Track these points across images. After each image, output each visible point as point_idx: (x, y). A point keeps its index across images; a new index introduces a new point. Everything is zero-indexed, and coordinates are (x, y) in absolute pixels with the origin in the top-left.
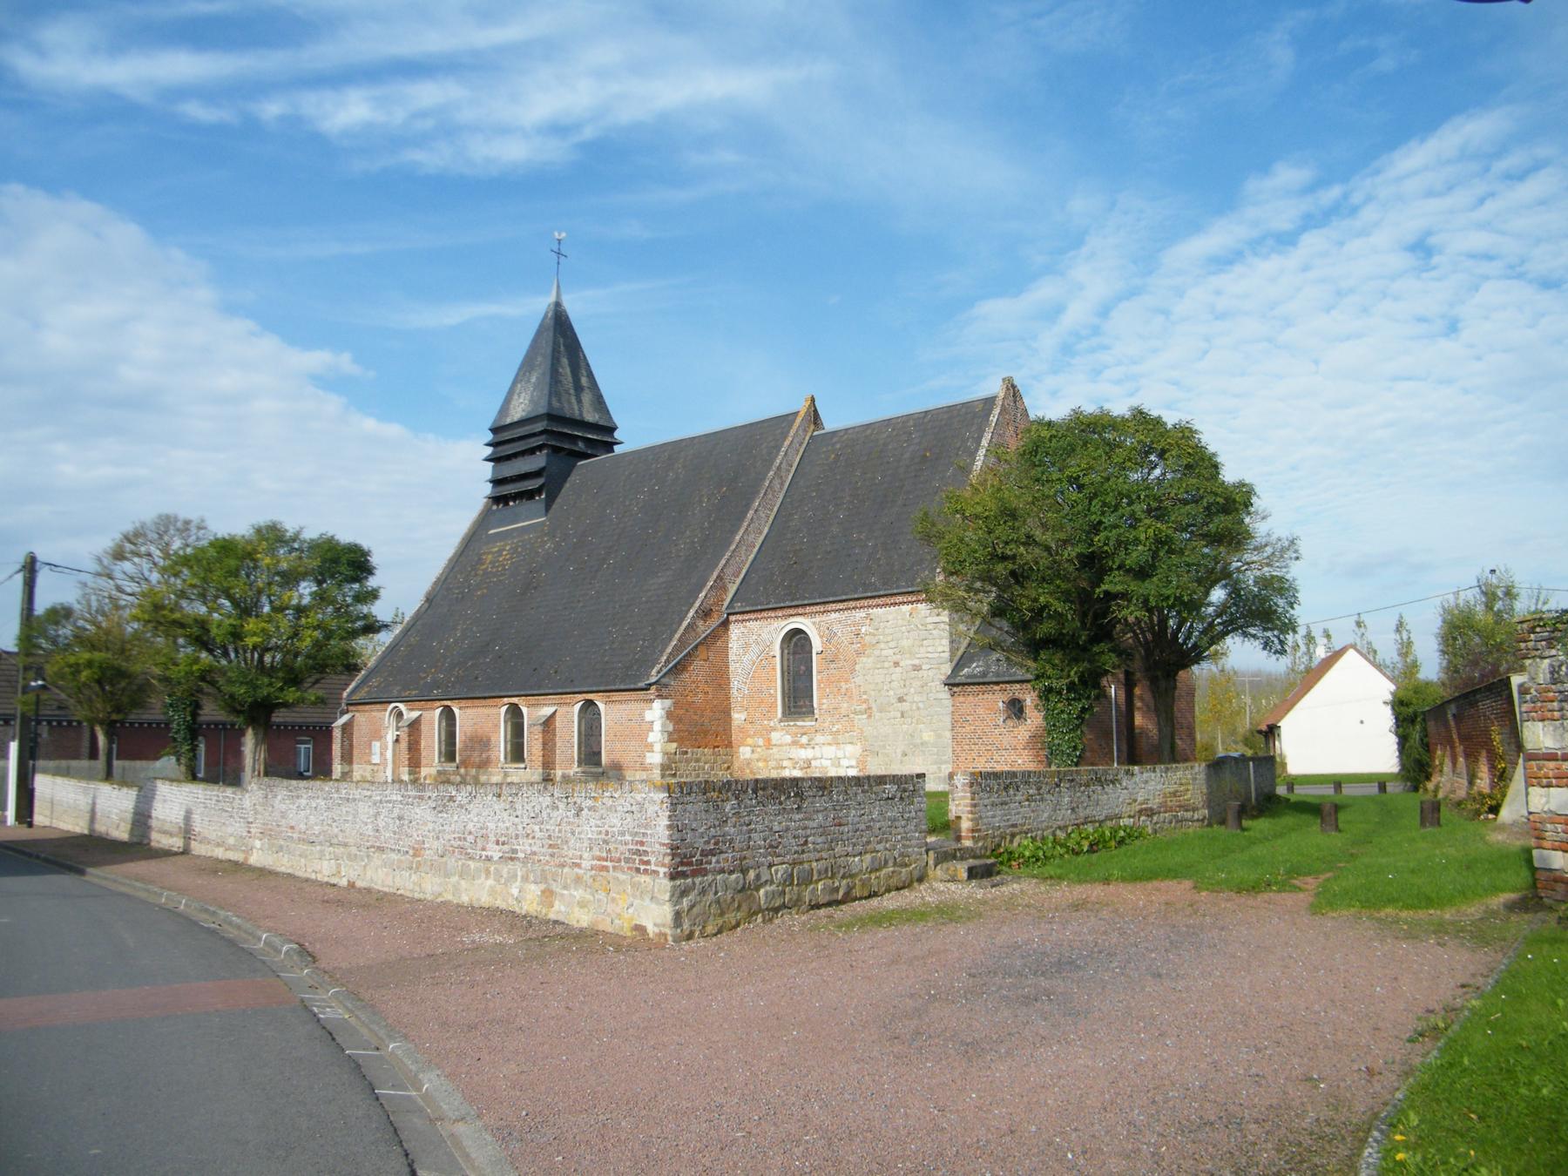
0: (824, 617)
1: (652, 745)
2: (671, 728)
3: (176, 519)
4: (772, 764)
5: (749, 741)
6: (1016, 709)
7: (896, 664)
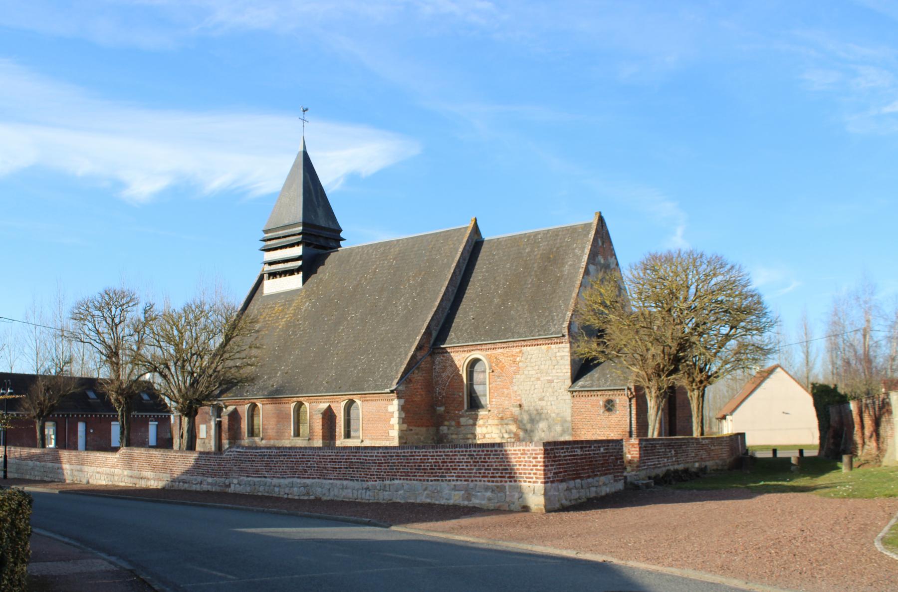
0: (494, 352)
1: (393, 426)
2: (403, 416)
3: (132, 300)
4: (461, 436)
5: (446, 423)
6: (609, 406)
7: (538, 379)
